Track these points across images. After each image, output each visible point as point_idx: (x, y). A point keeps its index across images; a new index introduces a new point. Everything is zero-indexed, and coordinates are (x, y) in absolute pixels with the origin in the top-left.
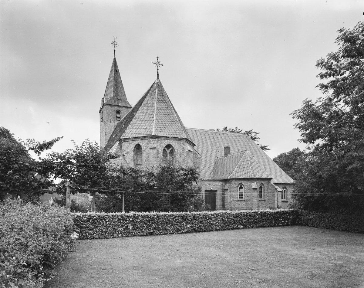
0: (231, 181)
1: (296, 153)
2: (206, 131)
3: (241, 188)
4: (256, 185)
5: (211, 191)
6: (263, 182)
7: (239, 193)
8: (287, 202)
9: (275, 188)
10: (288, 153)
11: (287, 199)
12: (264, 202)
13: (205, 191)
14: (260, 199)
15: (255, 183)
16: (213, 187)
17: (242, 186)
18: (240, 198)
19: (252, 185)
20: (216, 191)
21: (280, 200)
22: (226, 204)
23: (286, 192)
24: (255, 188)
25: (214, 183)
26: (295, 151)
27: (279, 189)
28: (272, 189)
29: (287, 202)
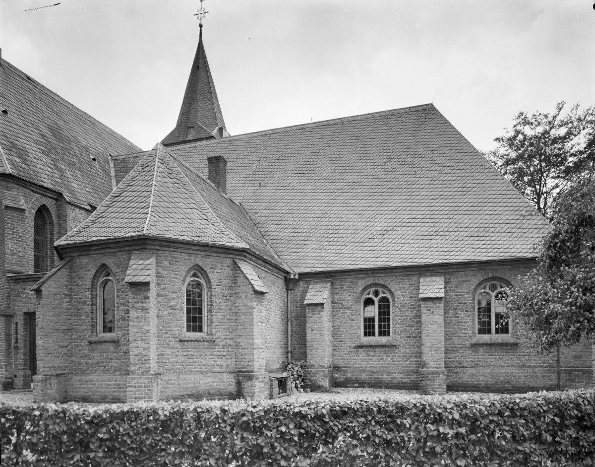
12: (111, 347)
18: (365, 335)
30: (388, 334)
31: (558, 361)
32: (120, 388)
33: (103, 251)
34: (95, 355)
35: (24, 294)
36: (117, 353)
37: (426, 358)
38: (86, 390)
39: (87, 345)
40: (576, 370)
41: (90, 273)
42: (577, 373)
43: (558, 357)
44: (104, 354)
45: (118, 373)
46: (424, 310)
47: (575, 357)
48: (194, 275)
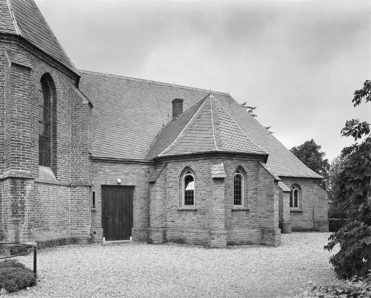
0: (167, 163)
1: (310, 147)
2: (150, 82)
3: (189, 179)
4: (223, 168)
5: (119, 187)
6: (243, 165)
7: (183, 193)
8: (300, 212)
9: (274, 179)
10: (298, 147)
11: (301, 207)
12: (244, 213)
13: (103, 187)
14: (236, 207)
15: (222, 165)
16: (124, 177)
17: (192, 175)
18: (186, 204)
19: (212, 169)
20: (132, 188)
21: (287, 208)
22: (152, 217)
23: (298, 193)
24: (218, 176)
25: (128, 168)
26: (308, 144)
27: (285, 187)
28: (267, 181)
29: (300, 212)
30: (193, 204)
31: (313, 218)
32: (251, 236)
33: (241, 159)
34: (235, 218)
35: (101, 171)
36: (248, 216)
37: (284, 218)
38: (232, 238)
39: (230, 212)
40: (321, 222)
41: (232, 170)
42: (322, 223)
43: (313, 217)
44: (240, 217)
45: (248, 228)
46: (284, 197)
47: (320, 217)
48: (237, 172)
